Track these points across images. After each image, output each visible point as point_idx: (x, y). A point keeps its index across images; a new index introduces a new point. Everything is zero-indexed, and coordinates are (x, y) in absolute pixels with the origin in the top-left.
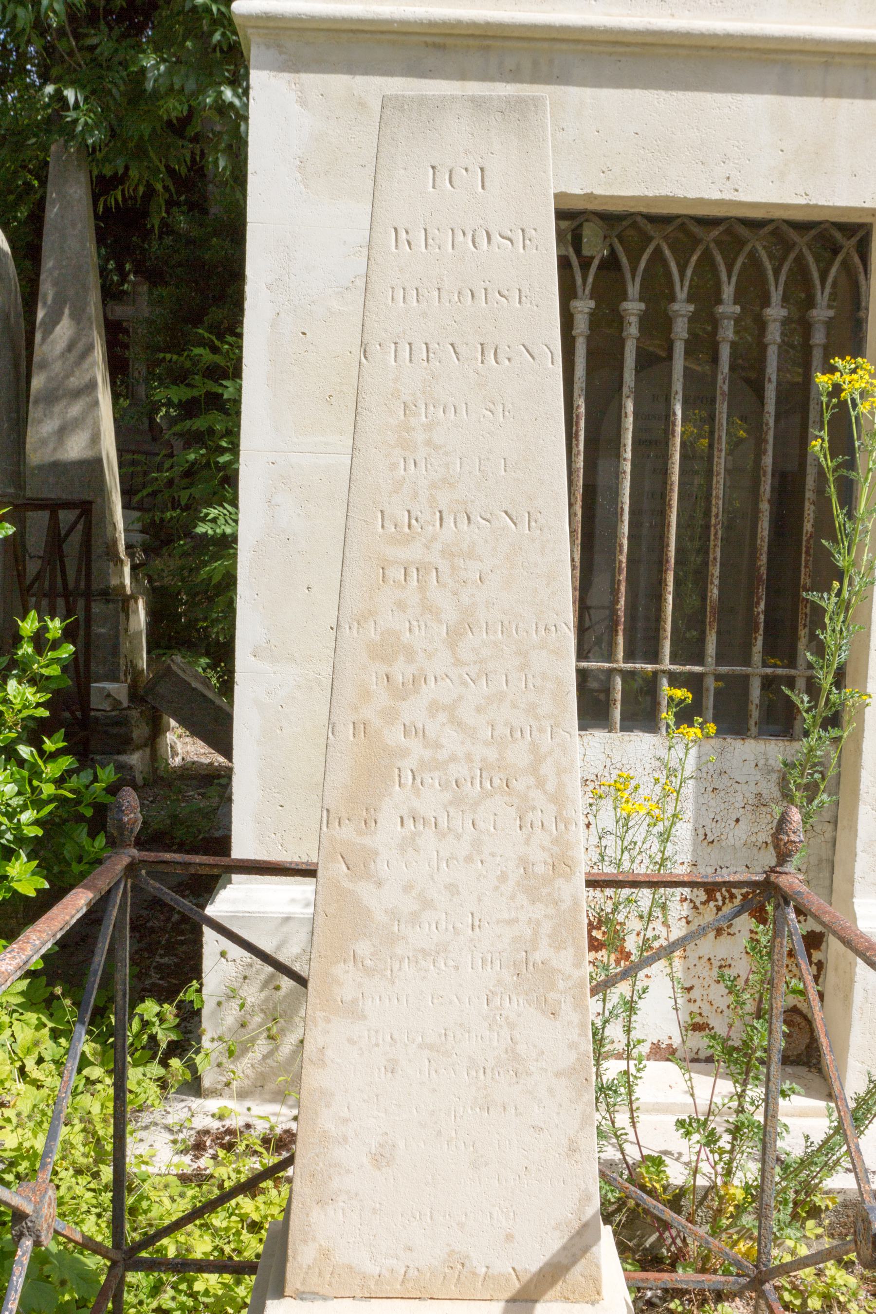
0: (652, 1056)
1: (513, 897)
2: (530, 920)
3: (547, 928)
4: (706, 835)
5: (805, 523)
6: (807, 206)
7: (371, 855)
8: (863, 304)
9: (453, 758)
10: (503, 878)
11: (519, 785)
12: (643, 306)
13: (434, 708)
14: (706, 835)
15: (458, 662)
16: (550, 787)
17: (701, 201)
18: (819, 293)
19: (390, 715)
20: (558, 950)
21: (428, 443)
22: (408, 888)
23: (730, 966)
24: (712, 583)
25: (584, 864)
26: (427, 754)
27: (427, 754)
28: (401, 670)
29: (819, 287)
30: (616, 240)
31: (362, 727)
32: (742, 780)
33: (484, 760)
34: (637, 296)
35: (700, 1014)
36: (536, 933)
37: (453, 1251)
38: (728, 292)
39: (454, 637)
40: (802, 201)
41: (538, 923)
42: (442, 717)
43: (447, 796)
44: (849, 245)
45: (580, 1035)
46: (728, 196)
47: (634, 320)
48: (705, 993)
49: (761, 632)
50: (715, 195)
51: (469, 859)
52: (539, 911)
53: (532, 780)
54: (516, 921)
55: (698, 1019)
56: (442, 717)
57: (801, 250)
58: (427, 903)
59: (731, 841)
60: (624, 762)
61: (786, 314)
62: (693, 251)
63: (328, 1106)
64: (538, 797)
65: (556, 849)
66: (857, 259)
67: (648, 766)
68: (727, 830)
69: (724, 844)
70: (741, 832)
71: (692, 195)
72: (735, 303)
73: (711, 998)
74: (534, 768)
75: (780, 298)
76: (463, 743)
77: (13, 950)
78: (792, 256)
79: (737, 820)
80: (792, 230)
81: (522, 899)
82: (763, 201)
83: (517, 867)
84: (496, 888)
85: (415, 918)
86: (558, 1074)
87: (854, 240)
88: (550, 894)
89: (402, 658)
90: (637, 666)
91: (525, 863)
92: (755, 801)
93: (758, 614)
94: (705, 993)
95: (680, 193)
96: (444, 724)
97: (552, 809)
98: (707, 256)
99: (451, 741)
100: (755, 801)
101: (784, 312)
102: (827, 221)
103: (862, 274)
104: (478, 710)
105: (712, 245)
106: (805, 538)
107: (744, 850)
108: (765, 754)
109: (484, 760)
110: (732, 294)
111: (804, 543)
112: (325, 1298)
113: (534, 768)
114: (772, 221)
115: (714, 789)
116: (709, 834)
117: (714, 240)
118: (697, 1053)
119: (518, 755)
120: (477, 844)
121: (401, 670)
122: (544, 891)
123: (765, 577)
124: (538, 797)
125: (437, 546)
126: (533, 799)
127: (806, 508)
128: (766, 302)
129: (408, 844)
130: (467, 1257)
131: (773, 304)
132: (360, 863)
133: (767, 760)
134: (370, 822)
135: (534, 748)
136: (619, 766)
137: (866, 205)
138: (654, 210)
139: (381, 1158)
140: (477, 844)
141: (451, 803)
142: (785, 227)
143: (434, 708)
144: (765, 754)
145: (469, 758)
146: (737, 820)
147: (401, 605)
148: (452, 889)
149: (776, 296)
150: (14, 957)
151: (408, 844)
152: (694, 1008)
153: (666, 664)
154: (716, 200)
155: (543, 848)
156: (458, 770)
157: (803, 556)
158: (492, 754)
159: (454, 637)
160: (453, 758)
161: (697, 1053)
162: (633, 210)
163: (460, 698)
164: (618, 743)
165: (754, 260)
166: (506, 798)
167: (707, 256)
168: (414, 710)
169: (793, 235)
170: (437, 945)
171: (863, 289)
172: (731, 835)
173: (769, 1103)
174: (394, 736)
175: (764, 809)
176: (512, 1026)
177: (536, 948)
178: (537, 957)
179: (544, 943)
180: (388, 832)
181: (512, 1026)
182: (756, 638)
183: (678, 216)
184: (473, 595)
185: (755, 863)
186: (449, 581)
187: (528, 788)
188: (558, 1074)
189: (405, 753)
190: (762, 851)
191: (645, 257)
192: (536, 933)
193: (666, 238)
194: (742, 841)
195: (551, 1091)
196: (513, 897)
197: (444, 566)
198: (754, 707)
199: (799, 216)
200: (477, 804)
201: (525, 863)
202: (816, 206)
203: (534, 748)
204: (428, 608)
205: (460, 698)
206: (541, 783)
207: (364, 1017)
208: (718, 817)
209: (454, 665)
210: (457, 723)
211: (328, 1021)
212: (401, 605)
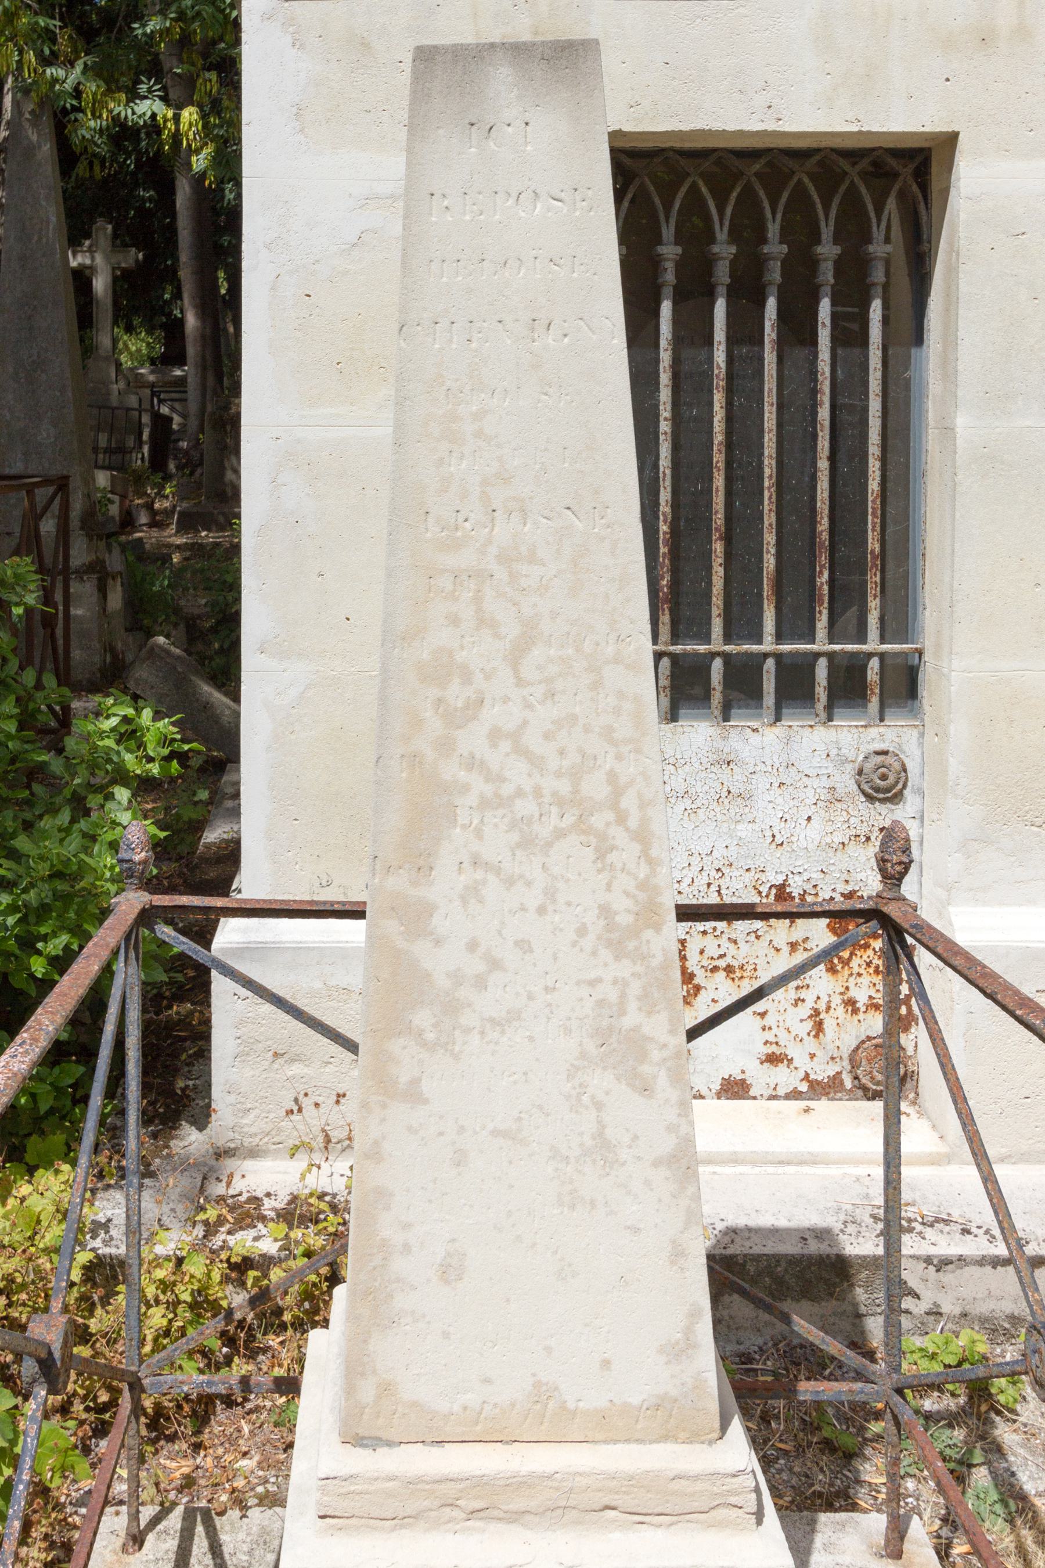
0: (723, 1094)
1: (594, 953)
2: (615, 982)
3: (635, 988)
4: (774, 836)
5: (870, 481)
6: (860, 133)
7: (428, 910)
8: (925, 237)
9: (520, 793)
10: (582, 931)
11: (599, 820)
12: (679, 250)
13: (495, 735)
14: (774, 836)
15: (520, 682)
16: (633, 822)
17: (741, 133)
18: (875, 229)
19: (445, 746)
20: (650, 1013)
21: (479, 434)
22: (472, 946)
23: (808, 986)
24: (768, 552)
25: (668, 903)
26: (488, 789)
27: (488, 789)
28: (456, 694)
29: (874, 220)
30: (646, 179)
31: (414, 759)
32: (812, 773)
33: (555, 794)
34: (672, 239)
35: (777, 1043)
36: (623, 996)
37: (539, 1382)
38: (773, 230)
39: (515, 657)
40: (854, 128)
41: (626, 984)
42: (505, 746)
43: (515, 837)
44: (906, 171)
45: (679, 1115)
46: (771, 126)
47: (670, 266)
48: (781, 1019)
49: (826, 605)
50: (754, 125)
51: (541, 910)
52: (625, 969)
53: (610, 816)
54: (599, 980)
55: (774, 1048)
56: (505, 746)
57: (852, 181)
58: (495, 964)
59: (803, 843)
60: (678, 756)
61: (839, 252)
62: (733, 187)
63: (387, 1208)
64: (619, 836)
65: (642, 896)
66: (915, 188)
67: (704, 760)
68: (798, 829)
69: (794, 846)
70: (814, 832)
71: (731, 127)
72: (781, 243)
73: (788, 1024)
74: (614, 802)
75: (831, 234)
76: (530, 775)
77: (24, 1043)
78: (843, 188)
79: (809, 818)
80: (841, 159)
81: (605, 954)
82: (811, 130)
83: (598, 918)
84: (574, 944)
85: (481, 983)
86: (657, 1163)
87: (911, 167)
88: (637, 949)
89: (458, 680)
90: (688, 647)
91: (605, 911)
92: (829, 797)
93: (822, 584)
94: (781, 1019)
95: (717, 126)
96: (507, 754)
97: (636, 848)
98: (748, 192)
99: (518, 773)
100: (829, 797)
101: (837, 250)
102: (881, 148)
103: (922, 204)
104: (547, 736)
105: (753, 179)
106: (870, 498)
107: (818, 853)
108: (837, 742)
109: (555, 794)
110: (777, 232)
111: (870, 504)
112: (390, 1444)
113: (614, 802)
114: (818, 150)
115: (782, 784)
116: (778, 836)
117: (756, 174)
118: (775, 1089)
119: (596, 787)
120: (550, 893)
121: (456, 694)
122: (631, 945)
123: (827, 543)
124: (619, 836)
125: (493, 550)
126: (614, 838)
127: (870, 465)
128: (815, 238)
129: (472, 894)
130: (556, 1389)
131: (824, 242)
132: (417, 918)
133: (840, 749)
134: (422, 867)
135: (612, 777)
136: (672, 760)
137: (927, 129)
138: (687, 145)
139: (450, 1271)
140: (550, 893)
141: (518, 845)
142: (834, 156)
143: (495, 735)
144: (837, 742)
145: (538, 792)
146: (809, 818)
147: (454, 620)
148: (524, 946)
149: (827, 232)
150: (27, 1052)
151: (472, 894)
152: (769, 1036)
153: (717, 643)
154: (758, 132)
155: (627, 894)
156: (526, 807)
157: (870, 517)
158: (564, 787)
159: (515, 657)
160: (520, 793)
161: (775, 1089)
162: (663, 146)
163: (525, 723)
164: (669, 735)
165: (800, 193)
166: (582, 838)
167: (748, 192)
168: (472, 739)
169: (844, 164)
170: (509, 1012)
171: (924, 219)
172: (802, 836)
173: (560, 834)
174: (451, 771)
175: (839, 805)
176: (599, 1106)
177: (622, 1013)
178: (628, 1022)
179: (632, 1005)
180: (445, 884)
181: (599, 1106)
182: (820, 612)
183: (714, 150)
184: (535, 605)
185: (832, 868)
186: (507, 589)
187: (608, 824)
188: (657, 1163)
189: (465, 788)
190: (839, 853)
191: (681, 194)
192: (623, 996)
193: (702, 175)
194: (816, 843)
195: (647, 1183)
196: (594, 953)
197: (501, 574)
198: (822, 689)
199: (849, 144)
200: (549, 845)
201: (605, 911)
202: (869, 133)
203: (612, 777)
204: (484, 622)
205: (525, 723)
206: (621, 819)
207: (426, 1101)
208: (786, 816)
209: (517, 685)
210: (521, 751)
211: (384, 1106)
212: (454, 620)
